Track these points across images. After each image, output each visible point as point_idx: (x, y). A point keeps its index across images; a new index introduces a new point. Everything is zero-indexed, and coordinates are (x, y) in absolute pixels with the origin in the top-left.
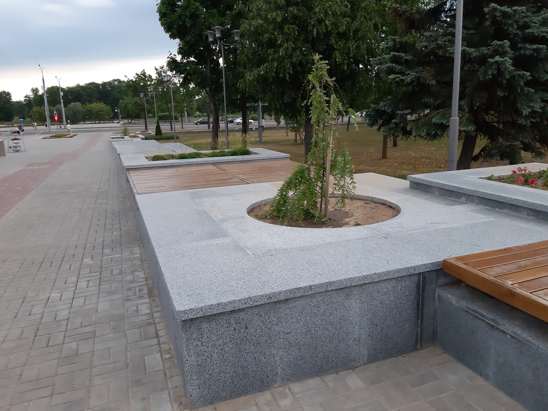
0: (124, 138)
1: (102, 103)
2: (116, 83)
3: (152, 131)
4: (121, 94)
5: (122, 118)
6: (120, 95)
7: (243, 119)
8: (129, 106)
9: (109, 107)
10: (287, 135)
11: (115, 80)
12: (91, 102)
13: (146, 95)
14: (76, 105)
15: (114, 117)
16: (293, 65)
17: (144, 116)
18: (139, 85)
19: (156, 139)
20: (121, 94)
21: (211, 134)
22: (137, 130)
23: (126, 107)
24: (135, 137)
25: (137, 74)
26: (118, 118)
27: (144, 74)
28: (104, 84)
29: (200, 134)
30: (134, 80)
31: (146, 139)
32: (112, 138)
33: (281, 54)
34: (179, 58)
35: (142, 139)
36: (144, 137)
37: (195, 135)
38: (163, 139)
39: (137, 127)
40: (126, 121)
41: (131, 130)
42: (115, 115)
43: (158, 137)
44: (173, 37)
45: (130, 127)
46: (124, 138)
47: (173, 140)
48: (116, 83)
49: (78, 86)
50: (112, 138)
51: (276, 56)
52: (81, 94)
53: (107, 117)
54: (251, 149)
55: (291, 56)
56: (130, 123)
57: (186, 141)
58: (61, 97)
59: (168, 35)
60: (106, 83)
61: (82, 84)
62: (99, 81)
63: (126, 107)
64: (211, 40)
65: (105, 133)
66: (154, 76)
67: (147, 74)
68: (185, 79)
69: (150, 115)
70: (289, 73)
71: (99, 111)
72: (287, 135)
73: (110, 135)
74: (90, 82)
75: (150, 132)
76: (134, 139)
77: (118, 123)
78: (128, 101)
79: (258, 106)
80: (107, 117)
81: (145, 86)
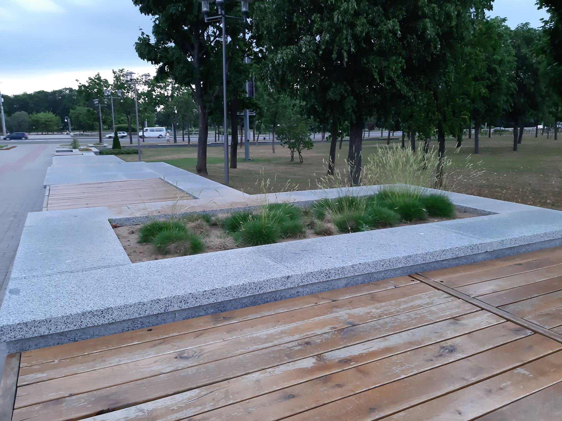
0: (72, 151)
1: (51, 113)
2: (67, 92)
3: (108, 144)
4: (73, 104)
5: (73, 130)
6: (71, 104)
7: (232, 129)
8: (81, 117)
9: (58, 117)
10: (274, 152)
11: (66, 89)
12: (38, 112)
13: (101, 102)
14: (22, 115)
15: (63, 128)
16: (355, 37)
17: (98, 128)
18: (91, 92)
19: (116, 154)
20: (73, 104)
21: (197, 149)
22: (90, 142)
23: (77, 117)
24: (87, 150)
25: (90, 79)
26: (68, 129)
27: (99, 79)
28: (54, 93)
29: (166, 149)
30: (87, 85)
31: (101, 153)
32: (57, 151)
33: (335, 19)
34: (153, 40)
35: (96, 153)
36: (97, 150)
37: (160, 149)
38: (122, 153)
39: (89, 140)
40: (78, 133)
41: (83, 142)
42: (65, 126)
43: (117, 150)
44: (145, 10)
45: (80, 140)
46: (72, 151)
47: (137, 156)
48: (67, 92)
49: (25, 95)
50: (57, 151)
51: (326, 24)
52: (28, 103)
53: (56, 128)
54: (457, 199)
55: (352, 26)
56: (82, 135)
57: (151, 156)
58: (1, 104)
59: (138, 7)
60: (56, 91)
61: (29, 92)
62: (49, 89)
63: (77, 117)
64: (204, 9)
65: (50, 146)
66: (111, 81)
67: (102, 78)
68: (161, 71)
69: (105, 127)
70: (349, 52)
71: (47, 121)
72: (274, 152)
73: (57, 147)
74: (39, 90)
75: (105, 145)
76: (86, 154)
77: (67, 134)
78: (81, 109)
79: (245, 115)
80: (56, 128)
81: (100, 91)
